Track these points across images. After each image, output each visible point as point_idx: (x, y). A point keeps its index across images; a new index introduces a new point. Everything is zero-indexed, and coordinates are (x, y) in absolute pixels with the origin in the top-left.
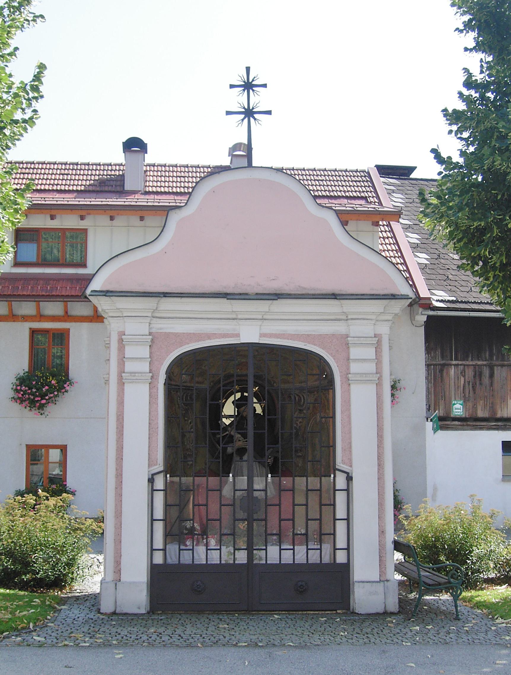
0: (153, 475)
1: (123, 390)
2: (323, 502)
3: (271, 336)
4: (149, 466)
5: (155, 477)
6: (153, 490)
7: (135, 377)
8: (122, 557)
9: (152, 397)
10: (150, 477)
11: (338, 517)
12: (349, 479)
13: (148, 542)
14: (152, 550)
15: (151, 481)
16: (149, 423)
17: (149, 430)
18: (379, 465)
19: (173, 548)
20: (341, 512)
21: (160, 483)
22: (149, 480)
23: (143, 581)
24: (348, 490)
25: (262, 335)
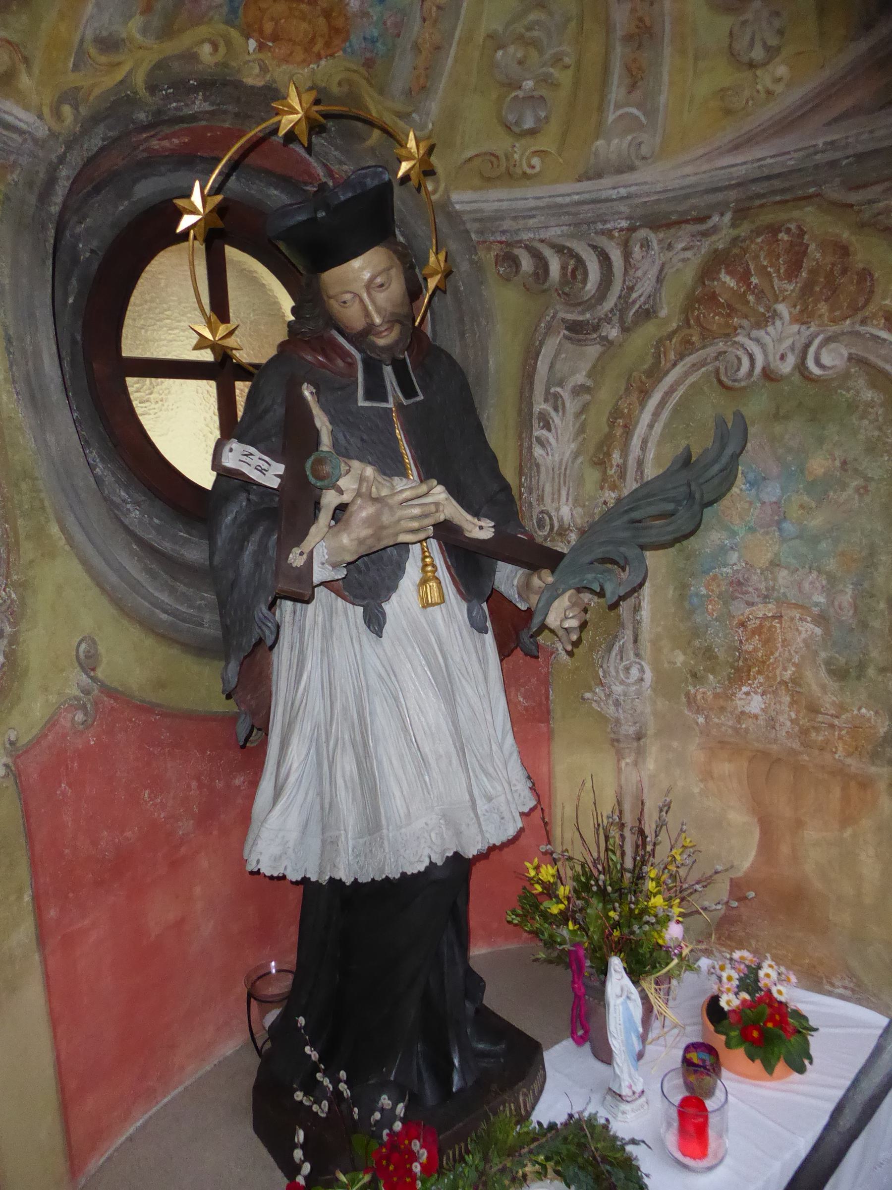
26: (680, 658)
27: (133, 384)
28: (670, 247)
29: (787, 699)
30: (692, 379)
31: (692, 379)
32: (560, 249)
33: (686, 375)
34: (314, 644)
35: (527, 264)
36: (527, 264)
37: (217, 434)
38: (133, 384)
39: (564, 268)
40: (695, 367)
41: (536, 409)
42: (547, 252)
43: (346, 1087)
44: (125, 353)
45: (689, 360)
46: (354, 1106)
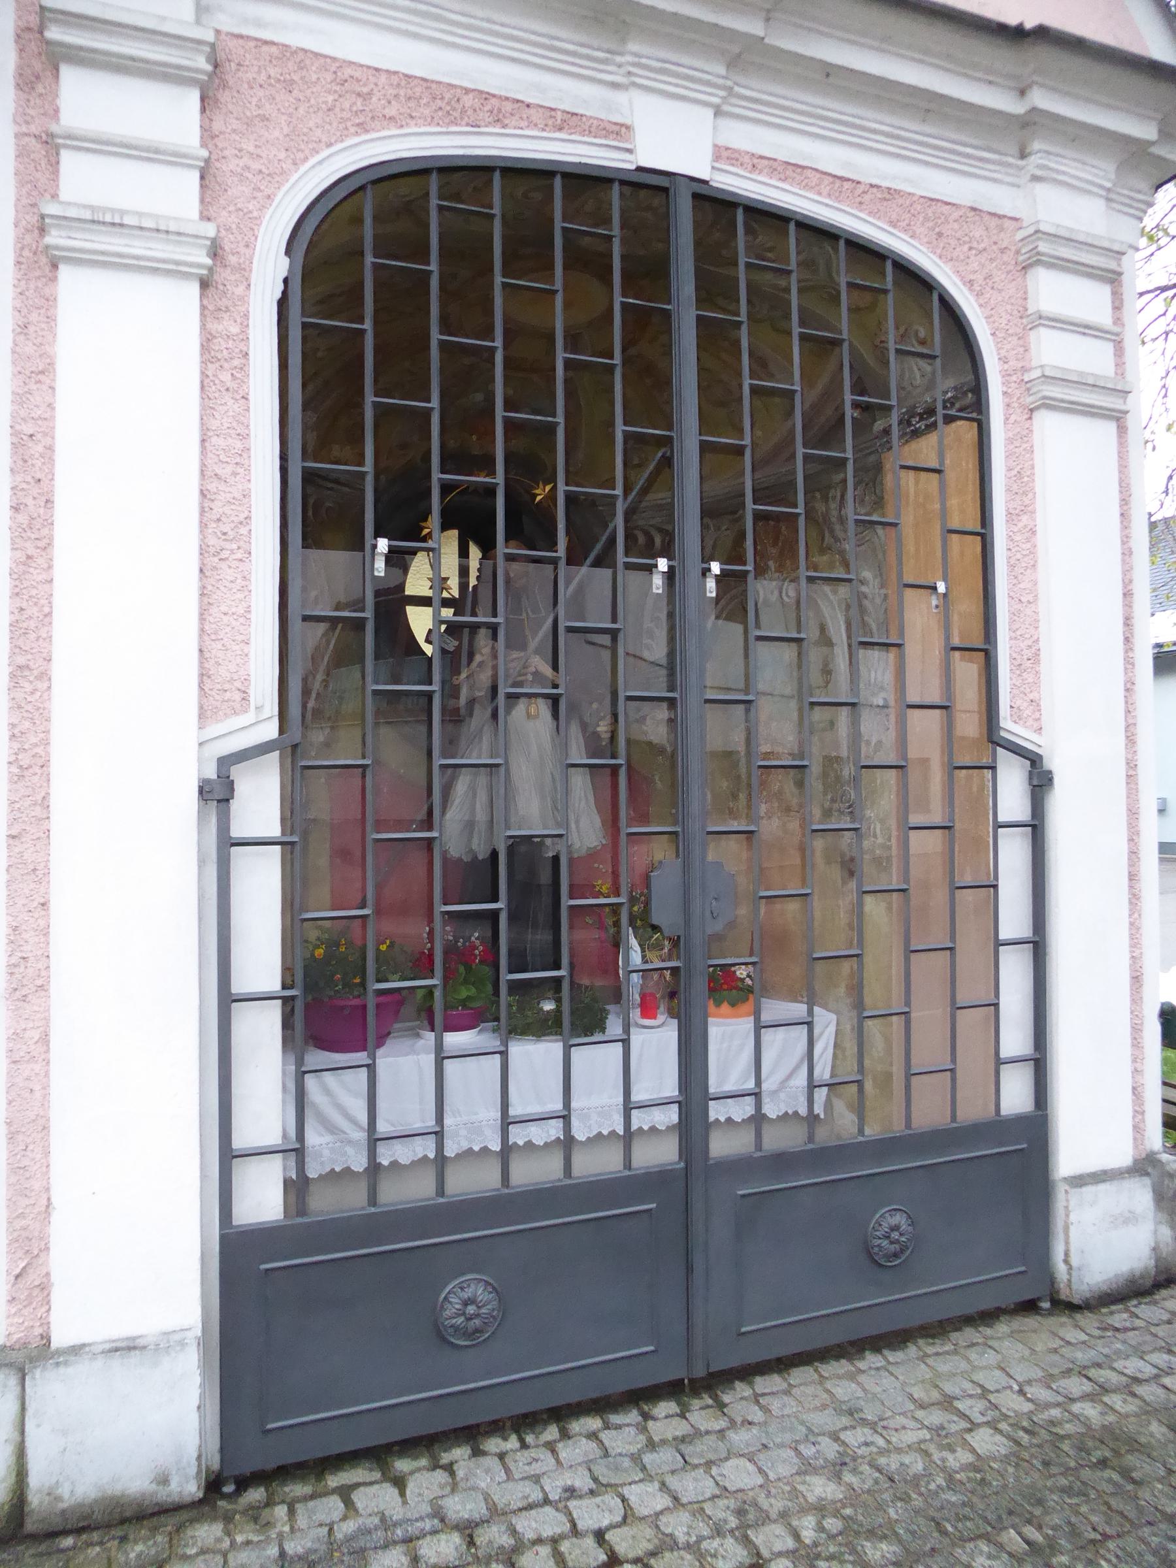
0: (226, 763)
1: (50, 301)
2: (961, 1000)
3: (757, 163)
4: (204, 716)
5: (236, 772)
6: (228, 843)
7: (120, 251)
8: (55, 1217)
9: (217, 354)
10: (211, 773)
11: (1004, 1053)
12: (1040, 782)
13: (201, 898)
14: (229, 1156)
15: (217, 794)
16: (203, 494)
17: (203, 526)
18: (1127, 640)
19: (339, 1089)
20: (1013, 919)
21: (260, 804)
22: (205, 791)
23: (172, 1322)
24: (1036, 828)
25: (722, 154)
26: (725, 784)
27: (410, 610)
28: (719, 529)
29: (776, 805)
30: (729, 607)
31: (729, 607)
32: (660, 530)
33: (727, 604)
34: (910, 547)
35: (641, 539)
36: (641, 539)
37: (396, 1491)
38: (410, 610)
39: (663, 541)
40: (732, 599)
41: (645, 626)
42: (654, 532)
43: (386, 550)
44: (407, 593)
45: (728, 596)
46: (378, 534)
